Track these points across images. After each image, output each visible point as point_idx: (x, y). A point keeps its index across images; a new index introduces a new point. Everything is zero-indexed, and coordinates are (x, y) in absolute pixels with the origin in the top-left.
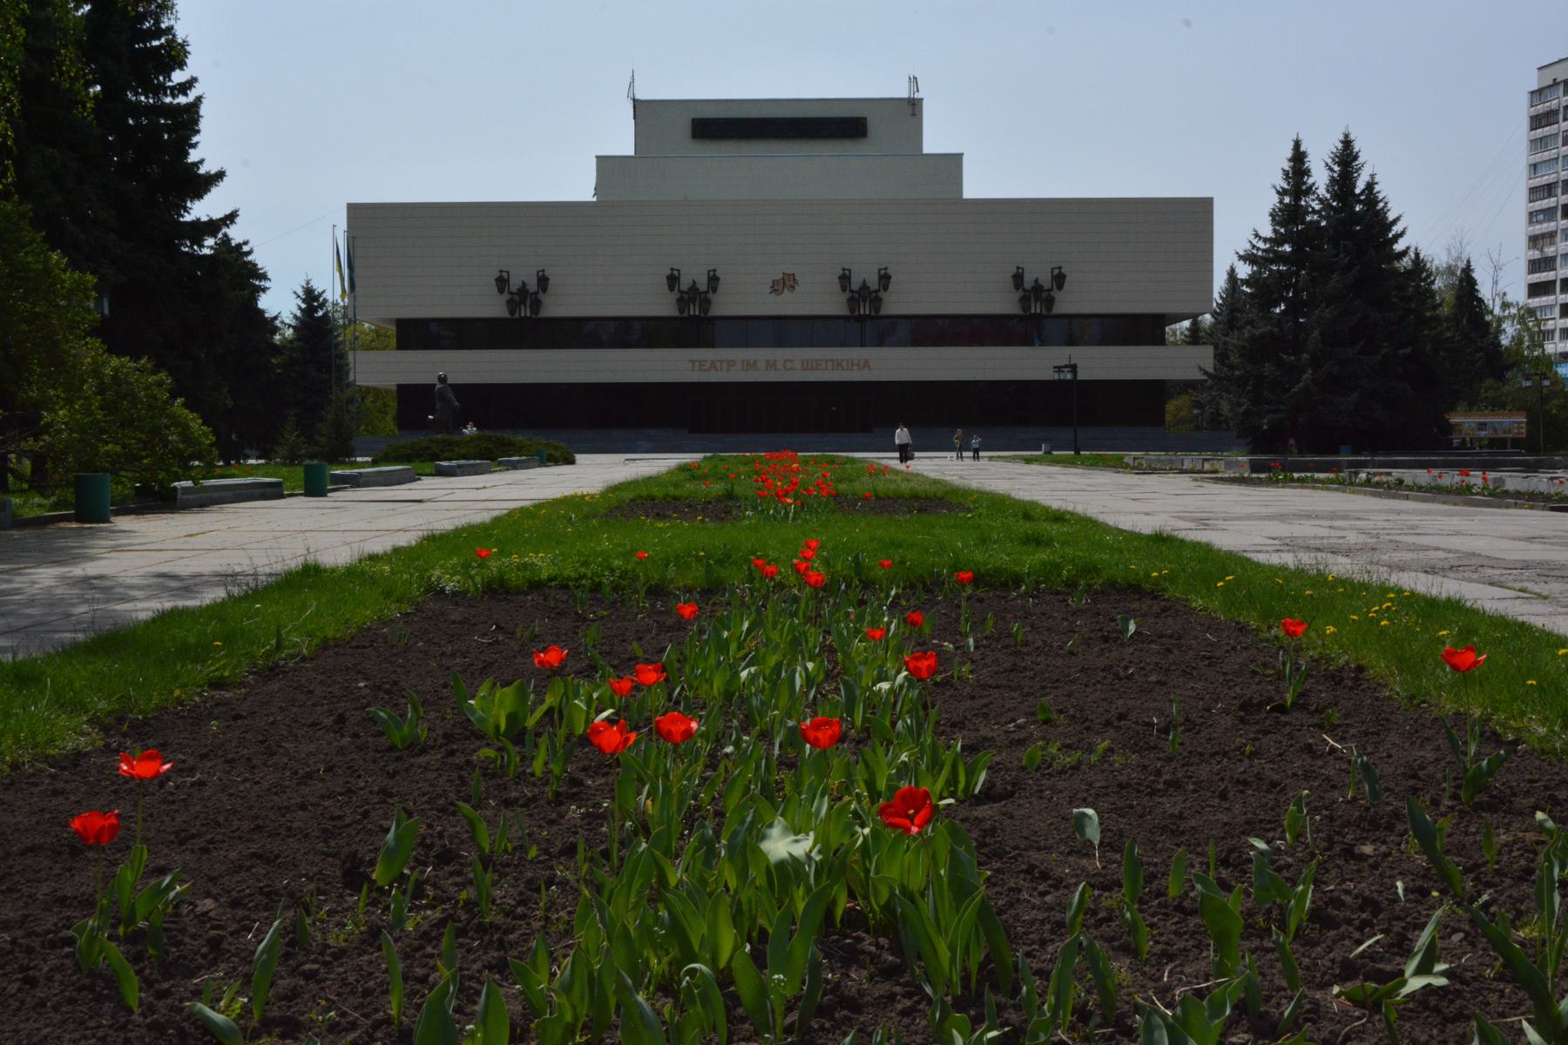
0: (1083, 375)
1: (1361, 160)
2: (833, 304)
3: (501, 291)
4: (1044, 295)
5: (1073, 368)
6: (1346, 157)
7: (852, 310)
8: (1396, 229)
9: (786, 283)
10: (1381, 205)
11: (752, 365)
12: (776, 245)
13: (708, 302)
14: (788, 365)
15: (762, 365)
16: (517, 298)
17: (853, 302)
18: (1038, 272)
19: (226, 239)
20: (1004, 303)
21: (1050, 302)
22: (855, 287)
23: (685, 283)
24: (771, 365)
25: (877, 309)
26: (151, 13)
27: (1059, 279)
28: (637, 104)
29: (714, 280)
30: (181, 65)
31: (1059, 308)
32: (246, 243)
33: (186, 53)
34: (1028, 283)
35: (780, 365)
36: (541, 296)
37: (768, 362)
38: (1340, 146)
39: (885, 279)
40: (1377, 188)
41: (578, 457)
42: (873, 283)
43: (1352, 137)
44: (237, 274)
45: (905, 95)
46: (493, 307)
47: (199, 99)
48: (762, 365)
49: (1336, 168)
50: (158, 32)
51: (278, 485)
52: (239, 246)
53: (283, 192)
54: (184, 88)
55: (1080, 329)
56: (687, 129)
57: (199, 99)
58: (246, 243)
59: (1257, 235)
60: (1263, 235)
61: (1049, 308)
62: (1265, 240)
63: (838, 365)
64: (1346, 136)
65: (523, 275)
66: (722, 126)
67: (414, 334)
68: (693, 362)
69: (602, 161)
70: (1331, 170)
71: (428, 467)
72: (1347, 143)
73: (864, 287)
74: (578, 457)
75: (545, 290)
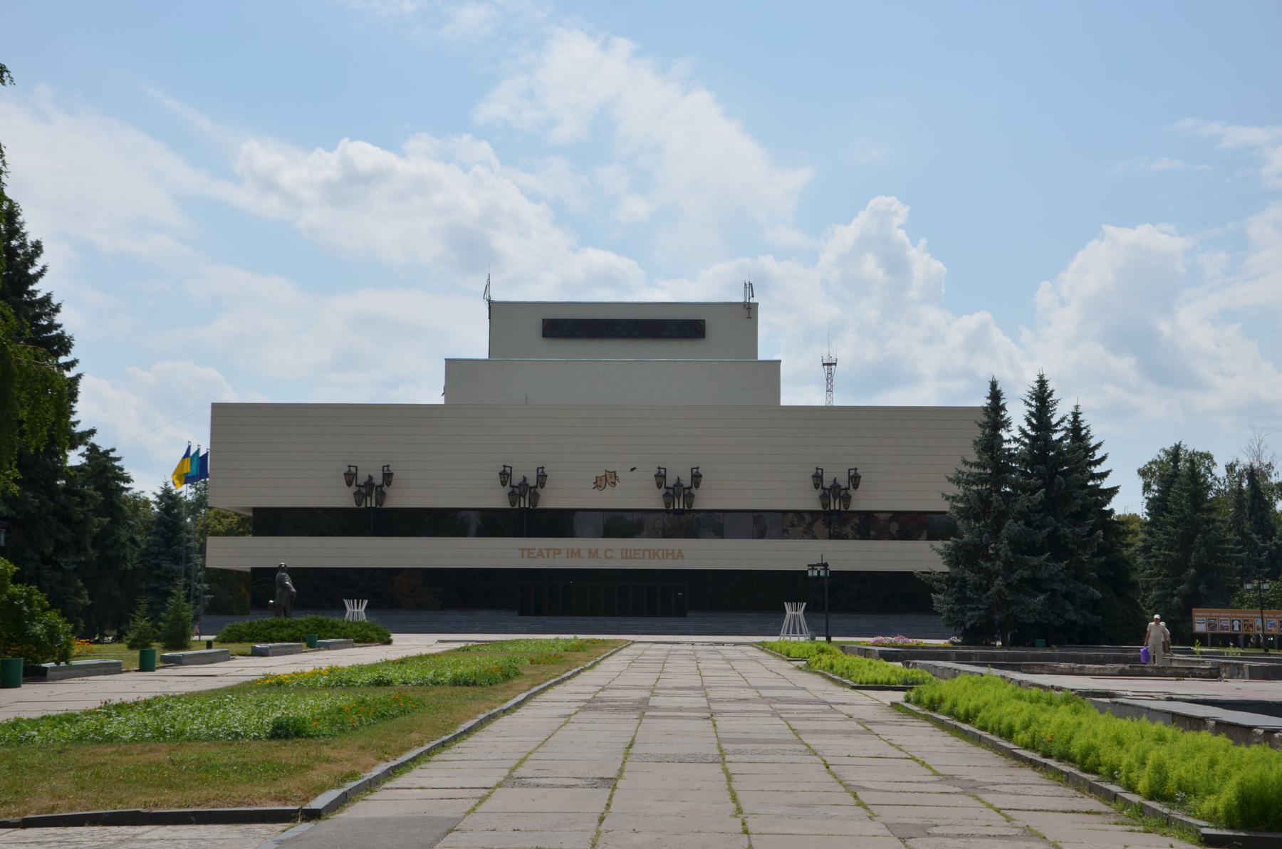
0: (832, 567)
1: (1054, 397)
2: (652, 499)
3: (349, 484)
4: (843, 493)
5: (826, 565)
6: (1042, 398)
7: (667, 505)
8: (1098, 454)
9: (607, 480)
10: (1084, 432)
11: (574, 553)
12: (602, 445)
13: (537, 496)
14: (609, 554)
15: (584, 554)
16: (363, 490)
17: (670, 495)
18: (836, 473)
19: (93, 448)
20: (809, 501)
21: (689, 497)
22: (361, 482)
23: (362, 478)
24: (593, 554)
25: (690, 505)
26: (45, 314)
27: (855, 479)
28: (492, 305)
29: (696, 478)
30: (66, 352)
31: (856, 505)
32: (113, 450)
33: (71, 345)
34: (827, 483)
35: (601, 554)
36: (385, 488)
37: (590, 551)
38: (1036, 385)
39: (696, 478)
40: (1081, 418)
41: (394, 636)
42: (687, 482)
43: (1045, 378)
44: (104, 470)
45: (742, 300)
46: (343, 498)
47: (79, 376)
48: (584, 554)
49: (1034, 403)
50: (52, 326)
51: (119, 664)
52: (107, 452)
53: (140, 416)
54: (69, 366)
55: (870, 526)
56: (710, 329)
57: (79, 376)
58: (113, 450)
59: (965, 462)
60: (969, 460)
61: (847, 506)
62: (977, 465)
63: (653, 554)
64: (1041, 377)
65: (370, 469)
66: (571, 326)
67: (269, 522)
68: (523, 550)
69: (451, 364)
70: (1030, 405)
71: (247, 647)
72: (1042, 383)
73: (678, 484)
74: (394, 636)
75: (389, 484)
